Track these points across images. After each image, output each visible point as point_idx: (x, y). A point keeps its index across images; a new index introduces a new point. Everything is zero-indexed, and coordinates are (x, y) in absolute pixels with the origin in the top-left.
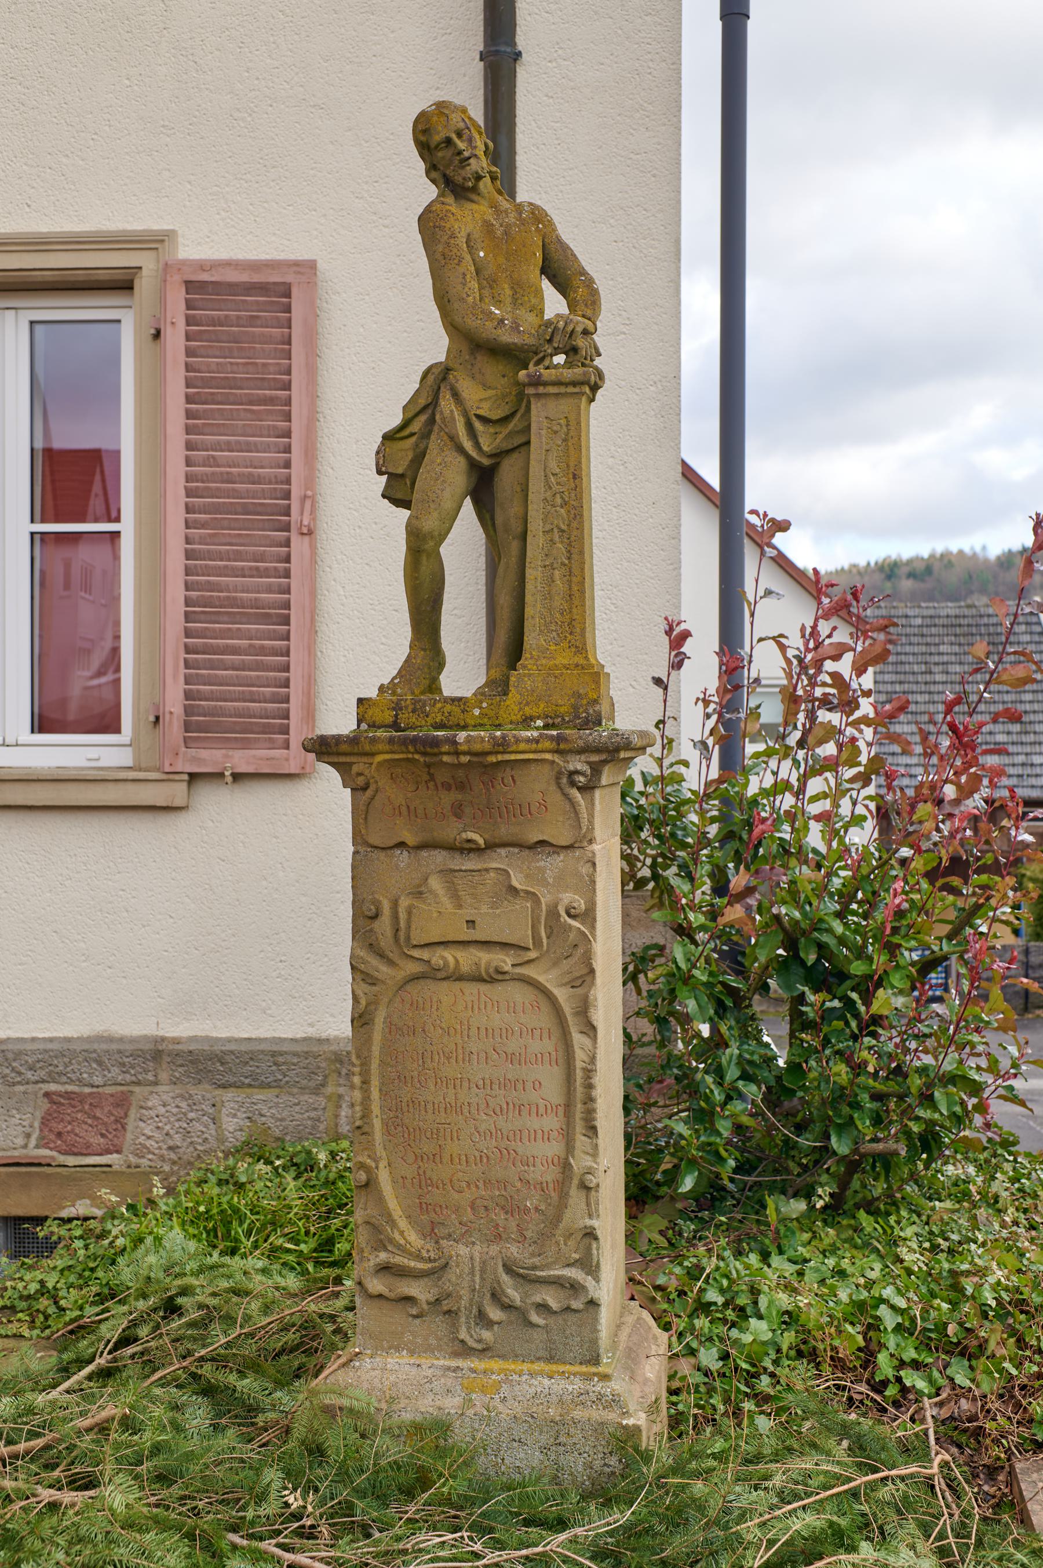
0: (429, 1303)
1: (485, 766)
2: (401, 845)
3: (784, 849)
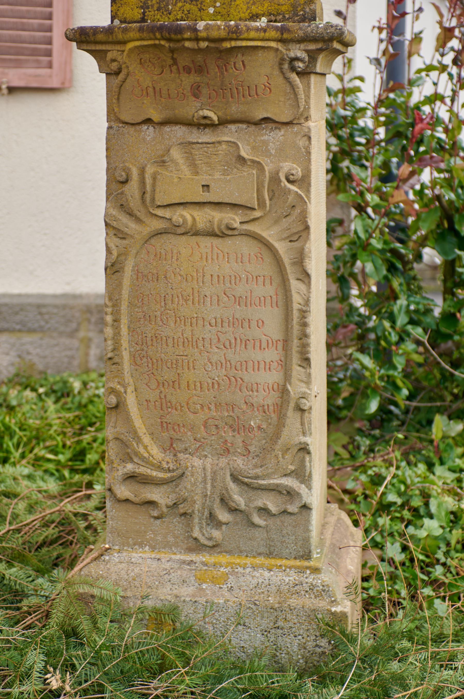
0: (168, 507)
1: (221, 52)
2: (148, 121)
3: (441, 146)
